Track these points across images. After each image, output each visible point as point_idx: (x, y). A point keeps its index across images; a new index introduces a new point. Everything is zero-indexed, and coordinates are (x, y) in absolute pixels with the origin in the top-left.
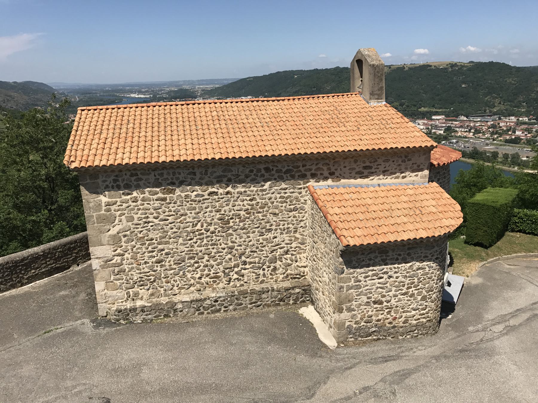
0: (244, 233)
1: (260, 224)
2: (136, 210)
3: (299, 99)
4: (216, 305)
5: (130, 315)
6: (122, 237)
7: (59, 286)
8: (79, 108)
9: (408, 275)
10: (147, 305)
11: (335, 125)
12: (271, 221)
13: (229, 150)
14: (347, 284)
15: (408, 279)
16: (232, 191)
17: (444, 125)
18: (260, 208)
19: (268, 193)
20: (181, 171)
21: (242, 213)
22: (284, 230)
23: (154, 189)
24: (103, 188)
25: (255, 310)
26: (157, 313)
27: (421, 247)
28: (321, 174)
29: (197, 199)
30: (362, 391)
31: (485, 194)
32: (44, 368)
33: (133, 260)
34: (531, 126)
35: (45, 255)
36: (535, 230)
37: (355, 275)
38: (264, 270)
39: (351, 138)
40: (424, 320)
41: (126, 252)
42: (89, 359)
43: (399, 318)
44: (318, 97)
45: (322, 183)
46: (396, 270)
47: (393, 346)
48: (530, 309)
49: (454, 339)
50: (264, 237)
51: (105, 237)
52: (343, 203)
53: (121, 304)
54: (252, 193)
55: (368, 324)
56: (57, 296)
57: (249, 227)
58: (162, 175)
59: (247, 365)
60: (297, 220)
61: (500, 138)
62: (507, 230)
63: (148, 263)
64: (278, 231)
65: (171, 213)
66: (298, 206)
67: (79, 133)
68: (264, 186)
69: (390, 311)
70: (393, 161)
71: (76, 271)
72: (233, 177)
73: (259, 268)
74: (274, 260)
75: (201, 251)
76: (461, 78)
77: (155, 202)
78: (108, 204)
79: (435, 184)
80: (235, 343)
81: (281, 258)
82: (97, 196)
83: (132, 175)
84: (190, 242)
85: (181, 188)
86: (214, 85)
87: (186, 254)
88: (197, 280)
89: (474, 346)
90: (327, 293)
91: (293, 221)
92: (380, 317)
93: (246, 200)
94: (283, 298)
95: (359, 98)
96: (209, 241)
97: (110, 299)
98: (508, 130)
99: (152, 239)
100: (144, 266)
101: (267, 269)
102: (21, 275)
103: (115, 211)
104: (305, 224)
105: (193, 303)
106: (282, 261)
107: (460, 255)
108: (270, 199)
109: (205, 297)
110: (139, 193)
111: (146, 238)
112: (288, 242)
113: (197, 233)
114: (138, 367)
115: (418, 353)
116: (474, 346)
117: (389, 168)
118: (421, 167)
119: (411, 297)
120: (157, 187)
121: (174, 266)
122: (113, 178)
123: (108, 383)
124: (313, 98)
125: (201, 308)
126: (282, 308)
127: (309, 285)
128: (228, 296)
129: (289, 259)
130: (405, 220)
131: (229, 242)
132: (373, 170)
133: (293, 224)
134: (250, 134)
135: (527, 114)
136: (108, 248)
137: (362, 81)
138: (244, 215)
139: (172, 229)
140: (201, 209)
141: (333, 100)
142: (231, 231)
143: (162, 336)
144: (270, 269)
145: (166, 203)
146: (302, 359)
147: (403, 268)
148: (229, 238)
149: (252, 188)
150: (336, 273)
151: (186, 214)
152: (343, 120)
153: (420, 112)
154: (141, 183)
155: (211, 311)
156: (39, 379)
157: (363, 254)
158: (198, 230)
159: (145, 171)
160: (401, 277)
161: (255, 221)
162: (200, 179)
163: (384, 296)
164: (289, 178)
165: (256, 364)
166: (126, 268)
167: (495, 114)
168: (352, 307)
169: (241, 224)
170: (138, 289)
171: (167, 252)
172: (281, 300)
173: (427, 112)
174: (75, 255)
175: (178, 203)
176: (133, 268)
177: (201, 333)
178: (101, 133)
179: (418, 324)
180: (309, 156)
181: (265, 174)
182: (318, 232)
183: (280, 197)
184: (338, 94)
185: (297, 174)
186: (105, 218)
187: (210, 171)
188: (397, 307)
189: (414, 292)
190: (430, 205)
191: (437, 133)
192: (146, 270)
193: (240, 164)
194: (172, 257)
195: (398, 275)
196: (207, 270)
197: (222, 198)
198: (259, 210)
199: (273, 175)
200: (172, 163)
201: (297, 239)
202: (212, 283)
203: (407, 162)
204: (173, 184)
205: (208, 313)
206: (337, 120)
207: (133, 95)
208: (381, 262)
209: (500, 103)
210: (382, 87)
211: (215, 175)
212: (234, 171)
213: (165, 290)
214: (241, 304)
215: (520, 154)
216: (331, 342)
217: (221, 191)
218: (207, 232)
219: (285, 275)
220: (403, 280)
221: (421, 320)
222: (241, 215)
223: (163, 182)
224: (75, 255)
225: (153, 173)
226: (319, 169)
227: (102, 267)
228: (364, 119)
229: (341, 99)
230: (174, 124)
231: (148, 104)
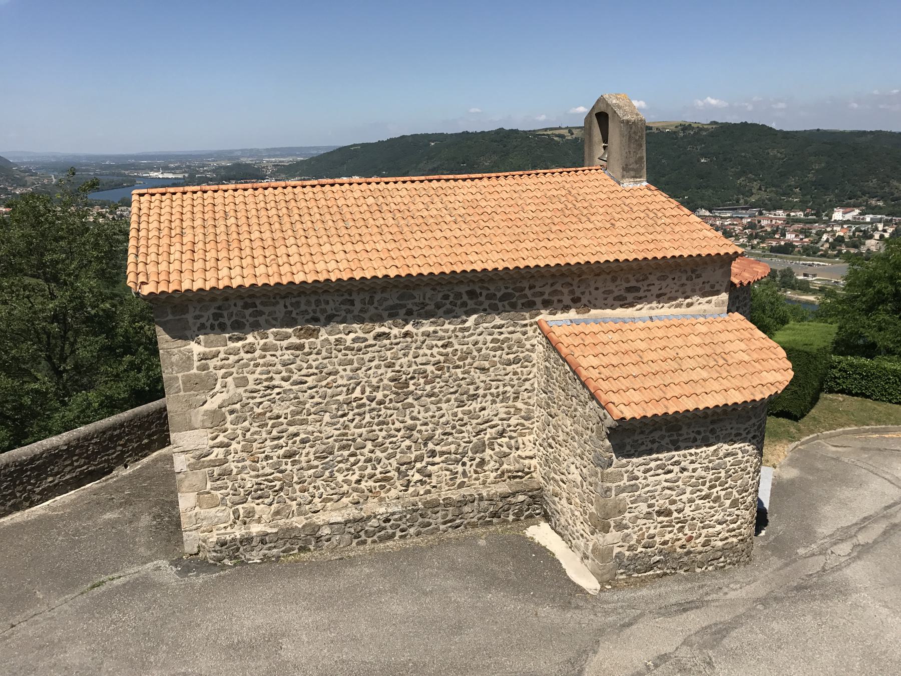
0: (432, 403)
1: (459, 386)
2: (251, 367)
4: (387, 528)
5: (241, 550)
6: (227, 414)
7: (99, 504)
8: (134, 192)
9: (711, 465)
10: (269, 531)
11: (574, 220)
12: (477, 381)
13: (410, 261)
15: (711, 472)
16: (414, 331)
19: (473, 334)
20: (329, 298)
21: (430, 368)
22: (498, 396)
23: (284, 330)
24: (195, 329)
25: (452, 534)
26: (288, 545)
28: (560, 301)
29: (356, 345)
30: (658, 662)
31: (788, 332)
32: (105, 650)
33: (245, 454)
34: (808, 226)
35: (71, 450)
36: (866, 389)
37: (630, 468)
38: (464, 464)
39: (605, 241)
40: (735, 540)
41: (233, 439)
42: (184, 630)
43: (697, 538)
44: (537, 174)
45: (560, 316)
46: (693, 458)
47: (689, 585)
48: (884, 517)
50: (466, 408)
51: (198, 415)
52: (599, 349)
54: (446, 334)
55: (649, 550)
56: (100, 521)
57: (440, 392)
58: (297, 304)
59: (458, 628)
60: (519, 379)
61: (762, 245)
62: (821, 390)
63: (271, 458)
64: (487, 398)
65: (311, 371)
66: (521, 355)
67: (143, 233)
68: (464, 322)
69: (683, 527)
70: (674, 279)
71: (125, 477)
72: (415, 308)
73: (457, 461)
74: (480, 448)
75: (360, 436)
76: (699, 147)
77: (284, 351)
78: (204, 357)
79: (737, 316)
80: (431, 592)
81: (492, 444)
82: (184, 342)
83: (246, 306)
84: (342, 420)
85: (329, 328)
86: (295, 158)
87: (335, 441)
88: (354, 485)
90: (578, 501)
91: (512, 380)
92: (667, 537)
94: (497, 511)
95: (602, 176)
96: (374, 418)
97: (205, 523)
98: (775, 232)
99: (278, 417)
100: (264, 463)
102: (29, 487)
103: (215, 368)
105: (349, 525)
106: (493, 450)
108: (476, 343)
109: (369, 514)
110: (258, 337)
111: (268, 414)
112: (505, 416)
113: (354, 404)
114: (273, 639)
115: (732, 595)
118: (717, 287)
119: (714, 501)
120: (288, 326)
121: (316, 463)
122: (213, 311)
124: (529, 175)
126: (496, 528)
127: (540, 489)
128: (408, 511)
130: (704, 374)
131: (407, 419)
132: (641, 294)
133: (513, 386)
134: (438, 234)
135: (802, 207)
137: (605, 147)
138: (432, 372)
139: (313, 397)
140: (362, 362)
142: (410, 400)
143: (303, 584)
144: (475, 463)
145: (304, 354)
146: (548, 613)
147: (704, 455)
148: (408, 412)
149: (446, 326)
150: (598, 465)
151: (337, 372)
152: (585, 212)
154: (262, 320)
155: (379, 537)
156: (100, 669)
157: (642, 433)
158: (356, 399)
161: (451, 381)
162: (361, 311)
163: (673, 502)
164: (507, 307)
165: (474, 624)
167: (753, 206)
168: (624, 522)
169: (428, 388)
170: (254, 505)
172: (495, 515)
174: (119, 448)
175: (324, 353)
177: (369, 576)
178: (182, 235)
181: (469, 302)
182: (558, 397)
183: (493, 341)
184: (568, 170)
185: (520, 302)
186: (197, 380)
187: (377, 297)
188: (693, 519)
189: (720, 493)
192: (268, 470)
193: (427, 285)
194: (312, 447)
195: (696, 465)
196: (370, 468)
197: (397, 344)
198: (458, 363)
199: (481, 304)
201: (518, 410)
202: (378, 489)
203: (696, 281)
204: (315, 320)
205: (374, 542)
206: (576, 212)
207: (153, 174)
208: (670, 446)
209: (760, 189)
210: (641, 158)
211: (386, 304)
214: (429, 524)
215: (794, 270)
216: (590, 584)
217: (395, 331)
218: (372, 401)
219: (499, 472)
220: (703, 474)
221: (730, 540)
223: (299, 318)
224: (119, 448)
225: (282, 302)
226: (555, 292)
228: (619, 209)
229: (573, 177)
230: (306, 218)
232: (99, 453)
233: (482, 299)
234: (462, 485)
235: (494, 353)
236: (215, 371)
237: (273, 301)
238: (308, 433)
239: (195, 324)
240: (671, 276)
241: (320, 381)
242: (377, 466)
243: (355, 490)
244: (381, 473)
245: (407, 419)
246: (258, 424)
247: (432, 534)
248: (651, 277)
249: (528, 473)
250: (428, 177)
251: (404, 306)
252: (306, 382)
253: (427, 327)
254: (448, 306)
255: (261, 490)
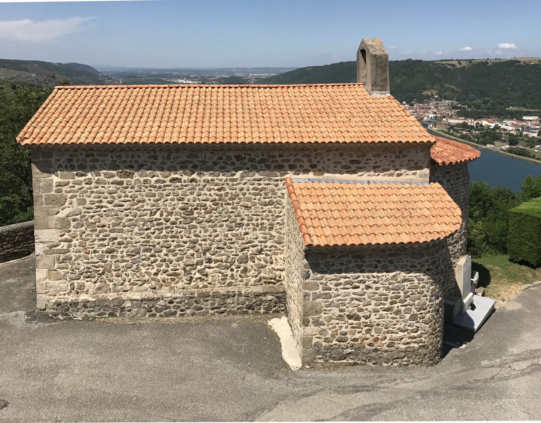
0: (209, 226)
2: (89, 193)
3: (294, 87)
4: (171, 307)
5: (70, 310)
6: (71, 221)
7: (10, 274)
9: (391, 286)
12: (242, 214)
14: (313, 291)
15: (392, 291)
16: (198, 178)
17: (538, 127)
18: (230, 199)
19: (239, 184)
20: (141, 154)
22: (258, 226)
23: (111, 172)
24: (56, 167)
25: (217, 317)
26: (102, 311)
27: (406, 255)
28: (301, 166)
29: (158, 185)
33: (81, 248)
37: (324, 281)
38: (232, 270)
40: (416, 345)
41: (74, 237)
43: (382, 340)
44: (316, 86)
45: (302, 176)
46: (376, 279)
47: (372, 374)
49: (456, 373)
50: (234, 232)
51: (53, 220)
53: (63, 296)
54: (220, 182)
55: (342, 343)
57: (216, 220)
58: (120, 157)
59: (183, 380)
63: (98, 252)
65: (127, 199)
66: (274, 200)
69: (370, 330)
70: (386, 157)
73: (227, 268)
74: (245, 260)
75: (159, 244)
77: (110, 185)
78: (59, 185)
80: (179, 353)
81: (253, 258)
82: (48, 175)
83: (87, 156)
84: (146, 232)
85: (140, 172)
87: (141, 245)
88: (152, 276)
89: (479, 384)
92: (357, 336)
93: (214, 189)
96: (168, 233)
97: (51, 290)
99: (104, 226)
100: (93, 255)
101: (235, 270)
103: (66, 192)
104: (282, 220)
105: (144, 302)
106: (254, 262)
107: (500, 274)
109: (159, 296)
111: (97, 224)
112: (262, 240)
113: (155, 223)
115: (402, 386)
116: (479, 384)
117: (381, 164)
120: (113, 170)
121: (127, 258)
122: (67, 157)
123: (14, 385)
124: (310, 87)
125: (153, 309)
126: (250, 317)
128: (186, 298)
129: (262, 260)
131: (192, 235)
132: (362, 165)
133: (268, 220)
136: (55, 232)
138: (210, 206)
139: (127, 216)
141: (337, 90)
142: (194, 223)
143: (99, 337)
145: (123, 187)
146: (253, 379)
147: (384, 278)
148: (192, 231)
149: (221, 177)
151: (144, 201)
153: (508, 111)
154: (97, 164)
155: (165, 313)
157: (333, 257)
158: (156, 219)
159: (102, 152)
160: (382, 289)
161: (223, 213)
162: (162, 163)
163: (361, 310)
164: (264, 168)
166: (72, 255)
168: (321, 320)
169: (207, 216)
170: (84, 281)
171: (119, 242)
172: (250, 307)
173: (517, 112)
175: (136, 188)
176: (80, 256)
177: (144, 337)
179: (408, 350)
180: (285, 146)
181: (236, 162)
183: (253, 189)
184: (338, 84)
185: (273, 165)
186: (54, 199)
187: (173, 155)
190: (424, 206)
191: (530, 136)
192: (95, 260)
194: (125, 247)
195: (378, 285)
196: (164, 265)
198: (228, 201)
199: (245, 164)
200: (130, 145)
201: (272, 237)
202: (169, 281)
204: (131, 167)
208: (356, 269)
210: (386, 79)
211: (179, 160)
212: (201, 157)
213: (115, 285)
214: (201, 309)
217: (185, 178)
218: (167, 221)
219: (258, 278)
221: (412, 345)
222: (208, 206)
223: (121, 165)
225: (110, 155)
226: (297, 160)
227: (46, 253)
231: (129, 86)
232: (22, 242)
233: (246, 161)
234: (230, 284)
235: (254, 197)
236: (66, 194)
237: (105, 153)
238: (123, 238)
239: (56, 164)
240: (383, 155)
241: (133, 206)
242: (170, 265)
243: (154, 279)
244: (172, 270)
245: (192, 235)
246: (90, 229)
247: (203, 315)
248: (368, 155)
249: (279, 281)
250: (240, 85)
251: (191, 162)
252: (123, 206)
253: (207, 176)
254: (223, 164)
255: (90, 272)
